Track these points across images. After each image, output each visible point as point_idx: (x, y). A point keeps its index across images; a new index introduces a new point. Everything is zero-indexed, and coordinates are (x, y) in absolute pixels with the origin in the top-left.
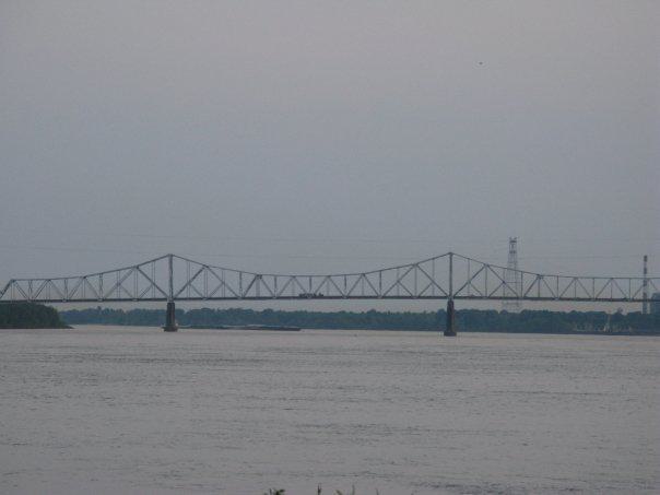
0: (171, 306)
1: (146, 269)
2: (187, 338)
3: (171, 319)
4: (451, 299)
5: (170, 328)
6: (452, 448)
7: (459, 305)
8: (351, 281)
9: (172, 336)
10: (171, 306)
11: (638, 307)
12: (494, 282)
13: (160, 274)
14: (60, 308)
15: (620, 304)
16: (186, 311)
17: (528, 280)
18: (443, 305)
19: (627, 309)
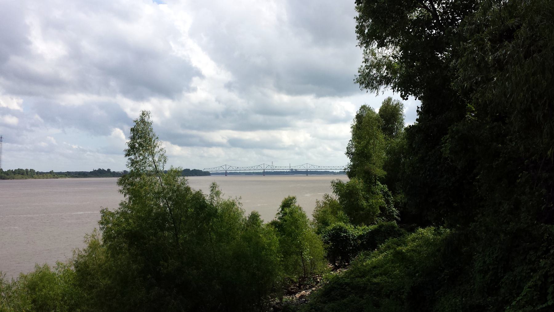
0: (226, 172)
1: (261, 166)
2: (228, 178)
3: (226, 174)
4: (264, 170)
5: (226, 175)
6: (5, 248)
7: (265, 171)
8: (337, 167)
9: (333, 179)
10: (226, 172)
11: (289, 170)
12: (270, 168)
13: (305, 166)
14: (211, 172)
15: (286, 170)
16: (36, 171)
17: (275, 167)
18: (263, 171)
19: (288, 171)
